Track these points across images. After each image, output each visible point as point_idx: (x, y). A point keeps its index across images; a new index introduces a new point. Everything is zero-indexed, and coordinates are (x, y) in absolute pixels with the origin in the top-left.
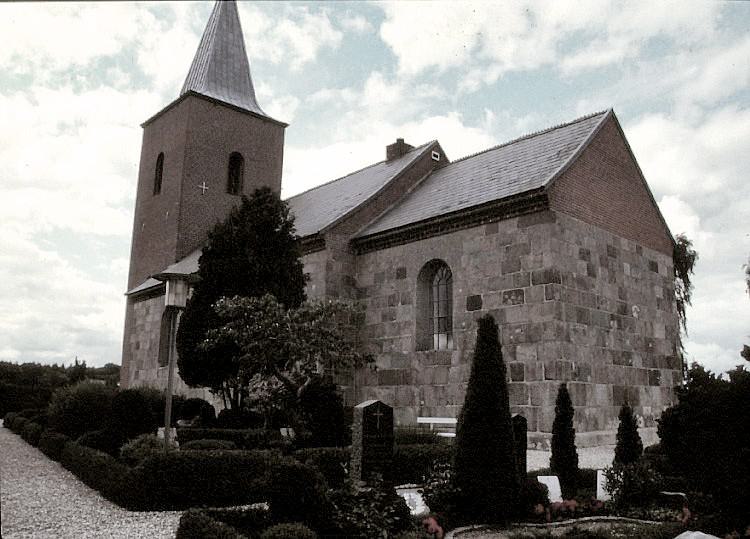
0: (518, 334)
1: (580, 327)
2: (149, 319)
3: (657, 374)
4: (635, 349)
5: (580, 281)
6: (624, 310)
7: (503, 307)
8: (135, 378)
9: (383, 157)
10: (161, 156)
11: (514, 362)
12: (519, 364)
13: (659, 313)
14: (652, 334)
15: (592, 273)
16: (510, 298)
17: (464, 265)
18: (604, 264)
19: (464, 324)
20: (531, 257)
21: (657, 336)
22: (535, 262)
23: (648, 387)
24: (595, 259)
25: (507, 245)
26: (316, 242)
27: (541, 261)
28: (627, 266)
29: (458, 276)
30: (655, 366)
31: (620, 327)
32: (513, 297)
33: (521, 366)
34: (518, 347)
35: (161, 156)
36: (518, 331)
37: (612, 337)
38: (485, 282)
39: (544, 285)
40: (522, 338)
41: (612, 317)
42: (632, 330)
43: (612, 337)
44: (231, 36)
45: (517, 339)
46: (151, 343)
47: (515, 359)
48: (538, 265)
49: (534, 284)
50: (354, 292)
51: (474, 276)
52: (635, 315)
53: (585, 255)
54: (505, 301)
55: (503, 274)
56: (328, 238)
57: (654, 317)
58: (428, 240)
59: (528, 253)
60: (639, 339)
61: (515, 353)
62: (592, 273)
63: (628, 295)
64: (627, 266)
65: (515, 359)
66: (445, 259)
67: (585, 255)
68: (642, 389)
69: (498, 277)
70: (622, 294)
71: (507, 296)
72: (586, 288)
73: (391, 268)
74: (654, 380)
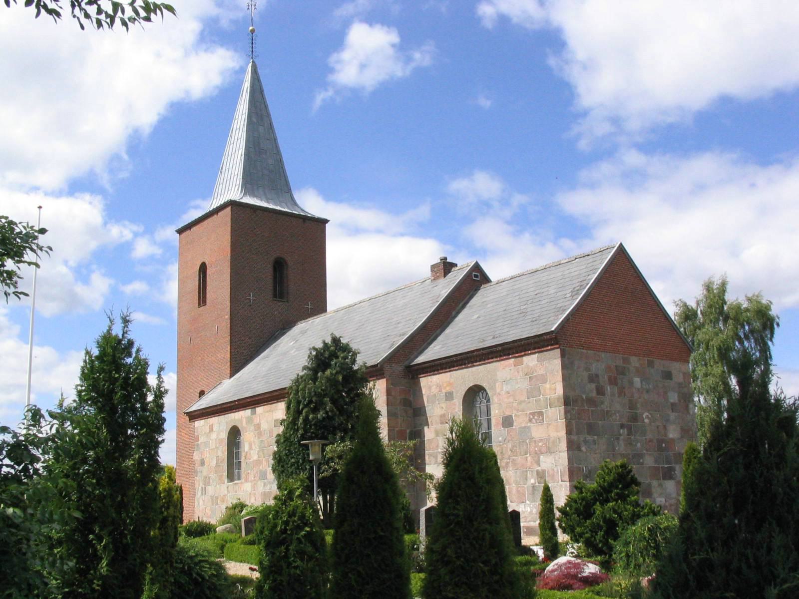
0: (541, 446)
1: (589, 438)
2: (214, 436)
3: (671, 469)
4: (647, 450)
5: (591, 402)
6: (635, 418)
7: (529, 425)
8: (202, 494)
9: (426, 272)
10: (203, 268)
11: (539, 468)
12: (542, 470)
13: (673, 416)
14: (666, 435)
15: (600, 391)
16: (534, 417)
17: (498, 391)
18: (613, 381)
19: (500, 439)
20: (548, 386)
21: (671, 436)
22: (550, 389)
23: (662, 481)
24: (604, 380)
25: (530, 376)
26: (376, 372)
27: (555, 389)
28: (637, 381)
29: (494, 400)
30: (668, 462)
31: (630, 433)
32: (536, 417)
33: (544, 471)
34: (542, 457)
35: (203, 268)
36: (540, 444)
37: (622, 443)
38: (515, 404)
39: (558, 408)
40: (544, 449)
41: (622, 426)
42: (644, 433)
43: (622, 443)
44: (261, 129)
45: (540, 450)
46: (217, 460)
47: (540, 466)
48: (553, 392)
49: (550, 407)
50: (410, 412)
51: (506, 400)
52: (646, 421)
53: (593, 378)
54: (530, 421)
55: (528, 398)
56: (387, 368)
57: (668, 421)
58: (470, 369)
59: (545, 383)
60: (651, 441)
61: (539, 460)
62: (600, 391)
63: (639, 406)
64: (637, 381)
65: (540, 466)
66: (484, 385)
67: (593, 378)
68: (655, 483)
69: (524, 401)
70: (632, 406)
71: (531, 417)
72: (596, 406)
73: (440, 391)
74: (668, 474)
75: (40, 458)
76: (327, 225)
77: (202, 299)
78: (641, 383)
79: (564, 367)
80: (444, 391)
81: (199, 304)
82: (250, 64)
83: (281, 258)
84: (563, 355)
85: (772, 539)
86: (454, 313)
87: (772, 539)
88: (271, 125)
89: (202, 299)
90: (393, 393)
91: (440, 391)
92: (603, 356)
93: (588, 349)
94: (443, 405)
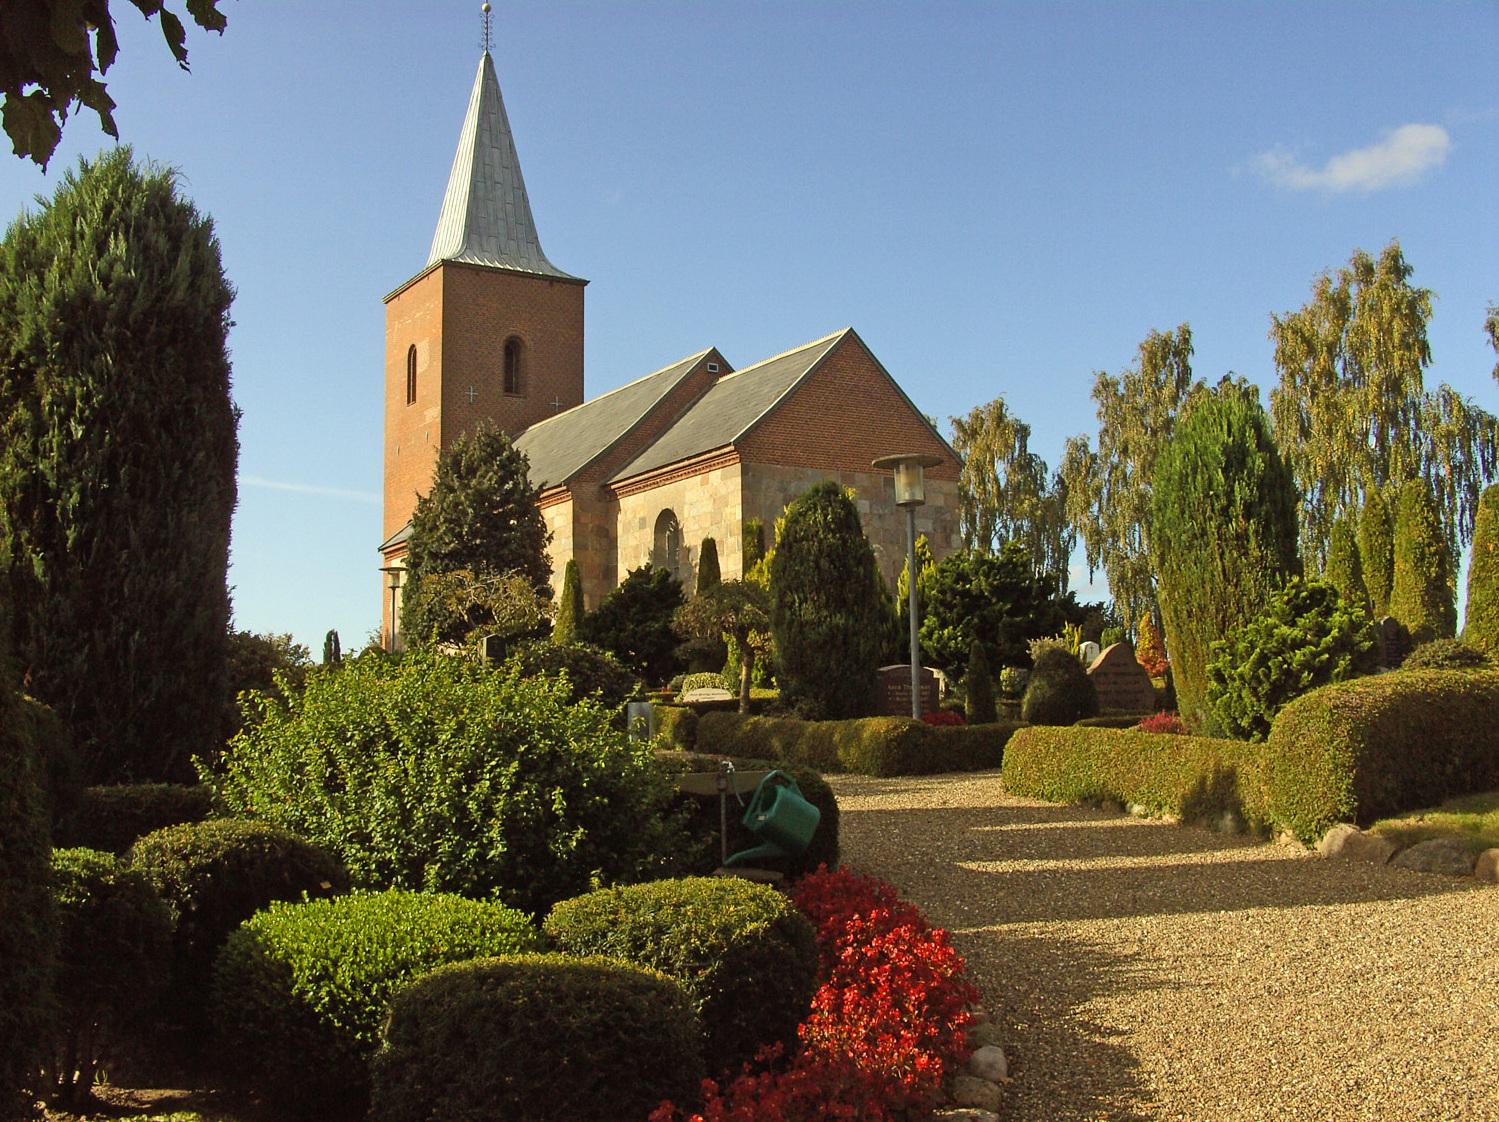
35: (413, 351)
73: (635, 517)
75: (1367, 828)
76: (585, 288)
77: (412, 396)
78: (871, 507)
79: (745, 487)
80: (638, 516)
81: (409, 402)
82: (483, 59)
83: (518, 337)
84: (744, 472)
85: (1257, 735)
86: (675, 418)
87: (1257, 735)
88: (511, 146)
89: (412, 396)
90: (583, 520)
91: (635, 517)
92: (810, 472)
93: (786, 463)
94: (637, 534)
